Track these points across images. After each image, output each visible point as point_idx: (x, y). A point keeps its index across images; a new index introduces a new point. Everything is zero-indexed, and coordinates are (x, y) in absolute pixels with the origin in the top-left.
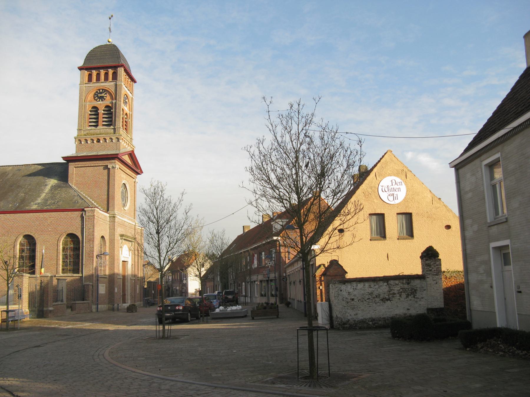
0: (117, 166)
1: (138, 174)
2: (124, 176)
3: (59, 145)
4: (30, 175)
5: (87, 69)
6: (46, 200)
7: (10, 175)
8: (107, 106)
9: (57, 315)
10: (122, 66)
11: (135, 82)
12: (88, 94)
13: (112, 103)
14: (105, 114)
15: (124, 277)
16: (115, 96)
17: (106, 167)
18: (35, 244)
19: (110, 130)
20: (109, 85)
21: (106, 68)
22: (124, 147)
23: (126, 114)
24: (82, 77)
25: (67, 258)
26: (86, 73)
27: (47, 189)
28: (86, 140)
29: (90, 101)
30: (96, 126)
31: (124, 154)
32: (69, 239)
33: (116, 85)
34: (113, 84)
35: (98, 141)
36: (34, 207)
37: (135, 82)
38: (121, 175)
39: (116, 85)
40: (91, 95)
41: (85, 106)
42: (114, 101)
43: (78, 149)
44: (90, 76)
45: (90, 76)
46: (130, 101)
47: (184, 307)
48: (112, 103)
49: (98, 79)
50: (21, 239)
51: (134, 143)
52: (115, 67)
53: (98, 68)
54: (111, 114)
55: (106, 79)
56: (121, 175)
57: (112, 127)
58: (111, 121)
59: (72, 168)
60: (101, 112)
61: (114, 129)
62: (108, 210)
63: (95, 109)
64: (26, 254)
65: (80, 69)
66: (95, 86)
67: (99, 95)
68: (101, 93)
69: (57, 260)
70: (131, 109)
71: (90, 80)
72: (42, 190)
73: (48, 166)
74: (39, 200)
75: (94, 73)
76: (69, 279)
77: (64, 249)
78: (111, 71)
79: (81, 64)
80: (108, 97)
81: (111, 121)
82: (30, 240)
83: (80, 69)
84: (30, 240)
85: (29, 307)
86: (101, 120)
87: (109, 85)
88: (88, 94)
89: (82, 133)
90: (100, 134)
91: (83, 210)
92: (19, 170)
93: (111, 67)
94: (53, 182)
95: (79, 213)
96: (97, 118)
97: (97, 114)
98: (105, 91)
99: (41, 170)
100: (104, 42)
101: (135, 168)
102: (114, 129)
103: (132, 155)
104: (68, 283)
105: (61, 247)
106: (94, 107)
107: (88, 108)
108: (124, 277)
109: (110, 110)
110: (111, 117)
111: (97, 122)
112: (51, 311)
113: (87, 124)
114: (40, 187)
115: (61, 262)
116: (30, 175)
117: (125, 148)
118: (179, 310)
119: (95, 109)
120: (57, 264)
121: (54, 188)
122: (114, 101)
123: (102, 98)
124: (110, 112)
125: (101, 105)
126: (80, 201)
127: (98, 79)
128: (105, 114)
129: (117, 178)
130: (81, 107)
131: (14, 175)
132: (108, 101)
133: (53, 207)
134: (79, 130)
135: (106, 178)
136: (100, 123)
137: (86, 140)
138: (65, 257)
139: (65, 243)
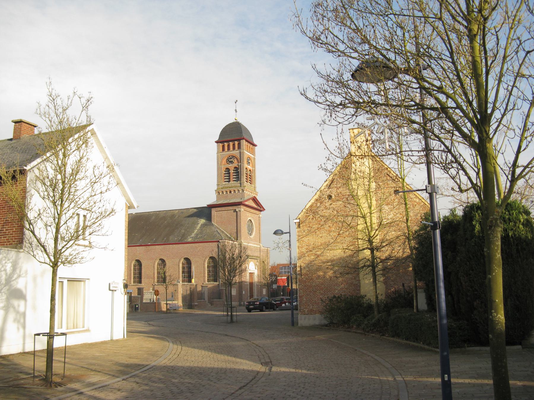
0: (242, 210)
1: (261, 211)
2: (248, 214)
3: (207, 196)
4: (189, 216)
5: (221, 142)
6: (197, 235)
7: (177, 217)
8: (235, 168)
9: (199, 307)
10: (243, 139)
11: (256, 146)
12: (222, 159)
13: (238, 165)
14: (234, 172)
15: (251, 284)
16: (240, 161)
17: (235, 211)
18: (191, 264)
19: (237, 184)
20: (236, 153)
21: (233, 141)
22: (248, 194)
23: (250, 170)
24: (218, 148)
25: (210, 272)
26: (221, 145)
27: (199, 227)
28: (223, 192)
29: (224, 165)
30: (229, 181)
31: (249, 200)
32: (211, 260)
33: (240, 152)
34: (238, 151)
35: (230, 192)
36: (190, 240)
37: (256, 146)
38: (246, 214)
39: (240, 152)
40: (225, 160)
41: (221, 168)
42: (239, 164)
43: (218, 198)
44: (223, 146)
45: (223, 146)
46: (253, 161)
47: (260, 303)
48: (238, 165)
49: (229, 149)
50: (182, 260)
51: (257, 190)
52: (239, 140)
53: (228, 141)
54: (238, 172)
55: (234, 148)
56: (246, 214)
57: (239, 182)
58: (238, 178)
59: (214, 211)
60: (232, 171)
61: (240, 183)
62: (237, 239)
63: (228, 170)
64: (186, 270)
65: (217, 142)
66: (227, 153)
67: (229, 160)
68: (231, 159)
69: (204, 274)
70: (254, 166)
71: (223, 150)
72: (196, 227)
73: (200, 209)
74: (193, 235)
75: (226, 144)
76: (210, 286)
77: (208, 266)
78: (236, 143)
79: (217, 139)
80: (236, 161)
81: (238, 178)
82: (188, 261)
83: (217, 142)
84: (188, 261)
85: (183, 302)
86: (231, 177)
87: (236, 153)
88: (222, 159)
89: (220, 187)
90: (232, 187)
91: (218, 241)
92: (182, 213)
93: (236, 140)
94: (202, 221)
95: (216, 244)
96: (229, 176)
97: (229, 173)
98: (233, 157)
99: (196, 213)
100: (232, 121)
101: (259, 207)
102: (240, 183)
103: (255, 200)
104: (209, 289)
105: (206, 265)
106: (227, 169)
107: (223, 170)
108: (251, 284)
109: (237, 170)
110: (238, 175)
111: (229, 179)
112: (196, 305)
113: (223, 180)
114: (195, 223)
115: (206, 275)
116: (189, 216)
117: (249, 195)
118: (257, 304)
119: (228, 170)
120: (204, 276)
121: (203, 225)
122: (239, 164)
123: (232, 162)
124: (237, 170)
125: (231, 167)
126: (218, 235)
127: (229, 149)
128: (234, 172)
129: (242, 217)
130: (219, 169)
131: (179, 216)
132: (235, 164)
133: (201, 240)
134: (218, 185)
135: (235, 218)
136: (231, 179)
137: (223, 192)
138: (209, 271)
139: (209, 263)
